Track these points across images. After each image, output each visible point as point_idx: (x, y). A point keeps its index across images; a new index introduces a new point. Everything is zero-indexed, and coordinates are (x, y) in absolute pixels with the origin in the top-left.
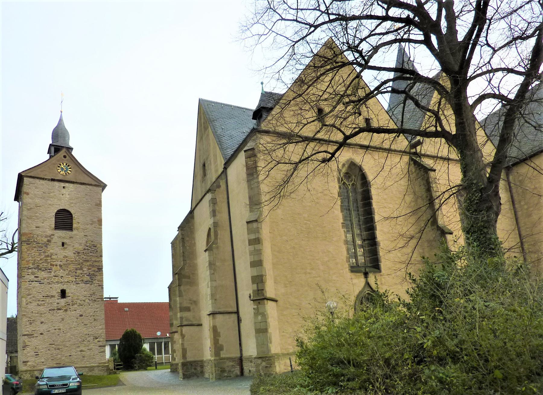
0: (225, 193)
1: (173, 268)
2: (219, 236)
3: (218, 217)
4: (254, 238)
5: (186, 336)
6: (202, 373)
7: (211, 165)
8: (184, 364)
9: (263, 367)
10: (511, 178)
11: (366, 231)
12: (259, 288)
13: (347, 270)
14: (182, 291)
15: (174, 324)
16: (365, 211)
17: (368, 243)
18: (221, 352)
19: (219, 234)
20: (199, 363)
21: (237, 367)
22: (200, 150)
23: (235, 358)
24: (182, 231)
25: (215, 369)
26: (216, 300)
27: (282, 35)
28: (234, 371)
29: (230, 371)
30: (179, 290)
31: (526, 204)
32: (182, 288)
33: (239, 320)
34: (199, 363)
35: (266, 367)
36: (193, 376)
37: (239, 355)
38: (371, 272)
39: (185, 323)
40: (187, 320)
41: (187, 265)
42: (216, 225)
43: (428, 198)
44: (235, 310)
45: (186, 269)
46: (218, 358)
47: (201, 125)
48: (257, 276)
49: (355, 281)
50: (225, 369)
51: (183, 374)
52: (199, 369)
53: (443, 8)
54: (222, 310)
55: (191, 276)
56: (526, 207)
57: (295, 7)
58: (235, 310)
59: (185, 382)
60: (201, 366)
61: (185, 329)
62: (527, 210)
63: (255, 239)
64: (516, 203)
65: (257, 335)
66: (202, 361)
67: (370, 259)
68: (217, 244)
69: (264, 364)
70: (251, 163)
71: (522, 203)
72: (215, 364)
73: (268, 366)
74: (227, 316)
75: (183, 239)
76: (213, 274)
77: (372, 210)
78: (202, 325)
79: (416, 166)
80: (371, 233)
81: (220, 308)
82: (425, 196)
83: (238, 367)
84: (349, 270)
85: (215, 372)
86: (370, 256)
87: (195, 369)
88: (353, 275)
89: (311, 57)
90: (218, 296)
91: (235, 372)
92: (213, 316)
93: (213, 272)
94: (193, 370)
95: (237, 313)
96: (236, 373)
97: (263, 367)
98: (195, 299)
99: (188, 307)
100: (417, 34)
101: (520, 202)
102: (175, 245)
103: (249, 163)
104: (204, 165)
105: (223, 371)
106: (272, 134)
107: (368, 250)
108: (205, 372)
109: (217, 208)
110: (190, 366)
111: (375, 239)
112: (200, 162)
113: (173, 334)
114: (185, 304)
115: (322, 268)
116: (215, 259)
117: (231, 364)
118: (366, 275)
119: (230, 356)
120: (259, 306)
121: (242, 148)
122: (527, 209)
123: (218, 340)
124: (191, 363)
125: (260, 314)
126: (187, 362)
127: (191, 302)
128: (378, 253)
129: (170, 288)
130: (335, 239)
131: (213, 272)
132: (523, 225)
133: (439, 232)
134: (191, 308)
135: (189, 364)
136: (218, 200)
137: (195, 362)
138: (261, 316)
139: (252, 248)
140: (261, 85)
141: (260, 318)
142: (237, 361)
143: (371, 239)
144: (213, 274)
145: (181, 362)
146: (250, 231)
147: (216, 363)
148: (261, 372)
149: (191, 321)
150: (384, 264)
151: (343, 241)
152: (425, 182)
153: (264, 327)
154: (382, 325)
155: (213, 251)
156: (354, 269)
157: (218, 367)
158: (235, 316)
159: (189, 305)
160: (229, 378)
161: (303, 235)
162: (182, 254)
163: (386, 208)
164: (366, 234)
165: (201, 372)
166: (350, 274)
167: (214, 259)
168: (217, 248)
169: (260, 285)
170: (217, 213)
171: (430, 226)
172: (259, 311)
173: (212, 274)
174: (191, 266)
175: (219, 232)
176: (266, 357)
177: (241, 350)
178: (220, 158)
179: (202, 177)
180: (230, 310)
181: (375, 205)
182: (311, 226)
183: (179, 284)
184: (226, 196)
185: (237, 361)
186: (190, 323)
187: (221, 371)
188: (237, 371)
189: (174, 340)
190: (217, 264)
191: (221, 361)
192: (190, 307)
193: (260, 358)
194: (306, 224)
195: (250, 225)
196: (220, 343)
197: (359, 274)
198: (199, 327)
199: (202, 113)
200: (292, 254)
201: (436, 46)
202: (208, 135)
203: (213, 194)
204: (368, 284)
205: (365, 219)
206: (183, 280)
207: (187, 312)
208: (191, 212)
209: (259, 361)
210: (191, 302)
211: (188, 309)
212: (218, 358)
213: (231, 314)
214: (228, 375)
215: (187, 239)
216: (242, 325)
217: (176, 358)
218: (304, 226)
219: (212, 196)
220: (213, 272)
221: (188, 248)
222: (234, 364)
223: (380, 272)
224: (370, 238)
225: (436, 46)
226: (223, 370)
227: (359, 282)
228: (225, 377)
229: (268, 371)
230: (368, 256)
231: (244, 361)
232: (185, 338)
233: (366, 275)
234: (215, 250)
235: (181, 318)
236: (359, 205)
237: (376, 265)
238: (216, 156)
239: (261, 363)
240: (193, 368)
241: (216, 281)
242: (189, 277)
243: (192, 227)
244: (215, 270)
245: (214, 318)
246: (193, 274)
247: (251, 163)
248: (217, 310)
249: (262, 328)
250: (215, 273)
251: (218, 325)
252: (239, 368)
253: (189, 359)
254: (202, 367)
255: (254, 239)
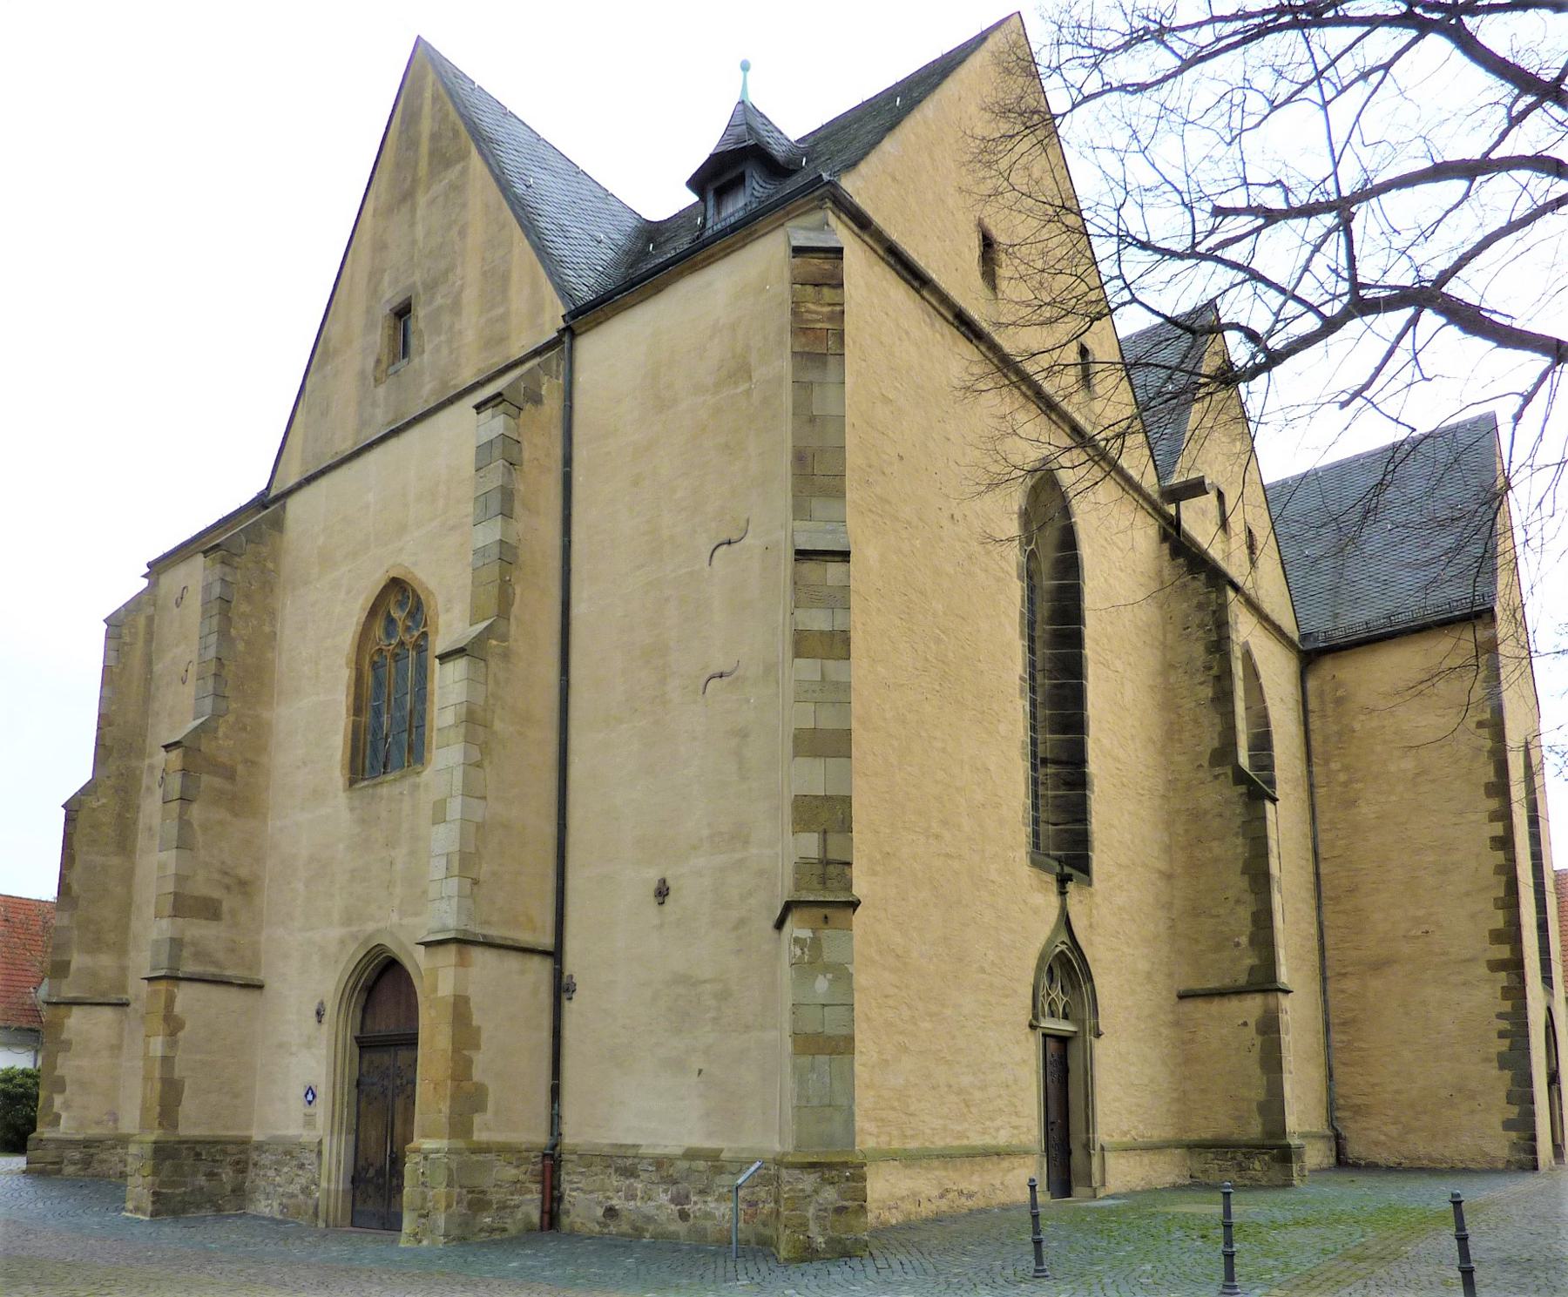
0: (557, 433)
1: (99, 728)
2: (515, 610)
3: (518, 526)
4: (826, 627)
5: (188, 1027)
6: (240, 1193)
7: (456, 307)
8: (162, 1152)
9: (825, 1210)
10: (1312, 684)
11: (1053, 732)
12: (832, 855)
14: (195, 826)
15: (73, 966)
16: (1056, 659)
17: (1057, 775)
18: (477, 1119)
19: (518, 597)
20: (230, 1148)
21: (531, 1192)
22: (380, 247)
23: (527, 1150)
24: (227, 569)
25: (448, 1195)
26: (476, 882)
28: (518, 1207)
29: (503, 1206)
30: (180, 818)
31: (1346, 768)
32: (196, 812)
33: (561, 989)
34: (231, 1148)
35: (840, 1210)
36: (199, 1207)
37: (541, 1138)
39: (189, 967)
40: (200, 955)
41: (231, 718)
42: (507, 555)
43: (1215, 671)
44: (547, 941)
45: (220, 733)
46: (460, 1144)
47: (411, 143)
48: (827, 798)
50: (489, 1197)
51: (155, 1194)
52: (227, 1175)
54: (495, 932)
55: (240, 768)
56: (1342, 777)
58: (547, 941)
59: (170, 1233)
60: (238, 1163)
61: (186, 995)
62: (1346, 786)
63: (832, 633)
64: (1314, 760)
65: (806, 1060)
66: (243, 1143)
67: (1058, 832)
68: (504, 638)
69: (830, 1194)
70: (819, 309)
71: (1334, 766)
72: (449, 1169)
73: (846, 1203)
74: (513, 962)
75: (225, 601)
76: (479, 765)
77: (1084, 660)
78: (260, 987)
79: (1181, 560)
80: (1070, 740)
81: (487, 923)
82: (1199, 663)
83: (536, 1187)
84: (1027, 853)
85: (448, 1206)
86: (1060, 821)
87: (211, 1175)
90: (484, 870)
91: (524, 1208)
92: (460, 953)
93: (479, 757)
94: (201, 1180)
95: (556, 954)
96: (527, 1215)
97: (825, 1210)
98: (243, 872)
99: (212, 900)
101: (1327, 762)
102: (125, 631)
103: (812, 307)
104: (403, 313)
105: (478, 1202)
106: (871, 236)
107: (1056, 797)
108: (255, 1190)
109: (520, 487)
110: (190, 1161)
111: (1084, 767)
112: (374, 292)
113: (62, 1010)
114: (201, 886)
116: (491, 701)
117: (511, 1173)
119: (509, 1140)
120: (826, 933)
121: (712, 256)
122: (1345, 784)
123: (469, 1063)
124: (197, 1148)
125: (827, 968)
126: (180, 1142)
127: (227, 880)
128: (1088, 816)
129: (73, 810)
131: (477, 756)
132: (1327, 827)
133: (1242, 789)
134: (225, 907)
135: (185, 1153)
136: (526, 455)
137: (214, 1142)
138: (830, 976)
139: (809, 669)
140: (742, 73)
141: (822, 984)
142: (534, 1164)
143: (1071, 763)
144: (479, 765)
145: (153, 1138)
146: (803, 595)
147: (454, 1166)
148: (813, 1229)
149: (216, 963)
150: (1101, 858)
151: (1020, 744)
152: (1209, 620)
153: (844, 1031)
155: (487, 666)
157: (461, 1187)
158: (540, 969)
159: (216, 894)
160: (502, 1241)
161: (928, 679)
162: (213, 667)
163: (1109, 667)
164: (1051, 740)
165: (233, 1191)
166: (1028, 868)
167: (486, 701)
168: (506, 656)
169: (833, 839)
170: (518, 508)
171: (1206, 764)
172: (821, 956)
173: (473, 765)
174: (244, 729)
175: (518, 590)
176: (845, 1165)
177: (555, 1120)
178: (535, 287)
179: (378, 361)
180: (526, 937)
183: (184, 787)
184: (558, 452)
185: (534, 1164)
186: (211, 970)
187: (470, 1205)
188: (530, 1207)
189: (64, 1036)
190: (498, 725)
191: (475, 1158)
192: (220, 902)
193: (813, 1166)
195: (808, 567)
196: (477, 1075)
198: (257, 993)
199: (428, 94)
200: (896, 744)
202: (457, 188)
203: (512, 422)
204: (1066, 922)
205: (1055, 686)
206: (206, 779)
207: (203, 922)
208: (268, 504)
209: (809, 1181)
210: (227, 880)
211: (209, 910)
212: (460, 1144)
213: (528, 956)
214: (496, 1225)
215: (245, 608)
216: (571, 1009)
217: (64, 1115)
219: (507, 427)
220: (479, 757)
221: (241, 646)
222: (522, 1177)
223: (1090, 884)
224: (1064, 757)
226: (480, 1200)
228: (481, 1230)
229: (850, 1229)
230: (1053, 819)
231: (566, 1168)
232: (181, 1034)
234: (494, 664)
235: (176, 944)
236: (1038, 633)
237: (1077, 857)
238: (505, 278)
239: (816, 1192)
240: (203, 1168)
241: (484, 798)
242: (230, 775)
243: (270, 565)
244: (485, 749)
245: (462, 963)
246: (251, 763)
247: (819, 309)
248: (479, 930)
249: (829, 1031)
250: (486, 763)
251: (473, 992)
252: (538, 1196)
253: (190, 1128)
254: (241, 1167)
255: (822, 633)
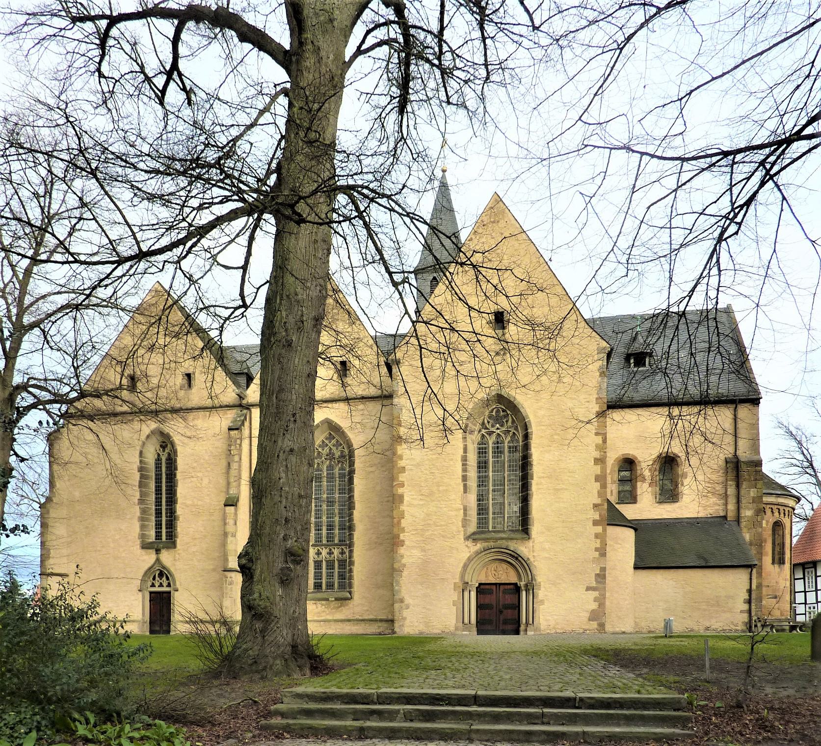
13: (139, 547)
27: (100, 230)
38: (163, 548)
49: (146, 557)
53: (243, 205)
57: (78, 111)
88: (143, 552)
89: (203, 120)
100: (718, 199)
115: (112, 545)
118: (158, 551)
130: (128, 517)
154: (156, 403)
156: (145, 546)
181: (181, 491)
182: (106, 505)
194: (100, 504)
197: (151, 551)
201: (196, 239)
204: (158, 560)
218: (99, 506)
223: (175, 547)
225: (196, 239)
227: (149, 558)
233: (158, 551)
